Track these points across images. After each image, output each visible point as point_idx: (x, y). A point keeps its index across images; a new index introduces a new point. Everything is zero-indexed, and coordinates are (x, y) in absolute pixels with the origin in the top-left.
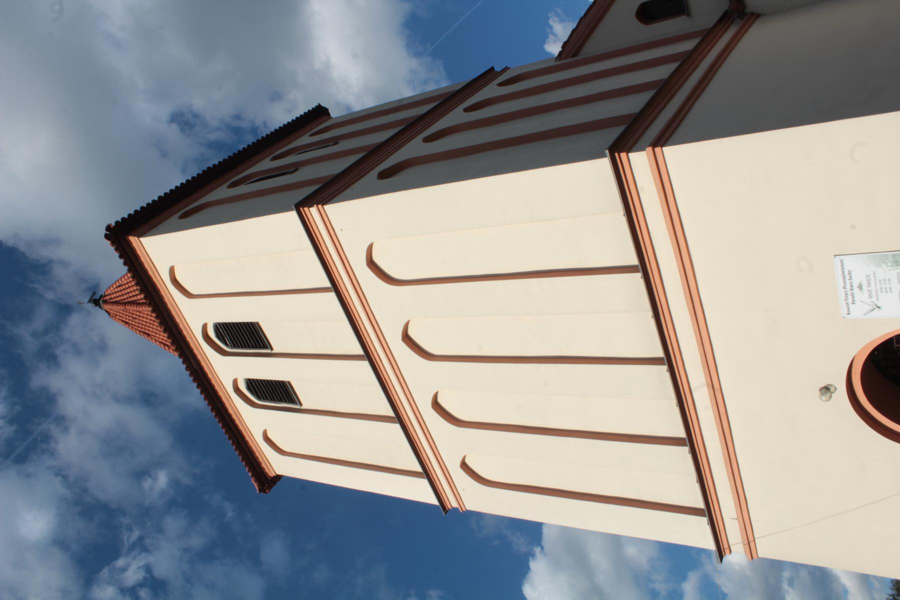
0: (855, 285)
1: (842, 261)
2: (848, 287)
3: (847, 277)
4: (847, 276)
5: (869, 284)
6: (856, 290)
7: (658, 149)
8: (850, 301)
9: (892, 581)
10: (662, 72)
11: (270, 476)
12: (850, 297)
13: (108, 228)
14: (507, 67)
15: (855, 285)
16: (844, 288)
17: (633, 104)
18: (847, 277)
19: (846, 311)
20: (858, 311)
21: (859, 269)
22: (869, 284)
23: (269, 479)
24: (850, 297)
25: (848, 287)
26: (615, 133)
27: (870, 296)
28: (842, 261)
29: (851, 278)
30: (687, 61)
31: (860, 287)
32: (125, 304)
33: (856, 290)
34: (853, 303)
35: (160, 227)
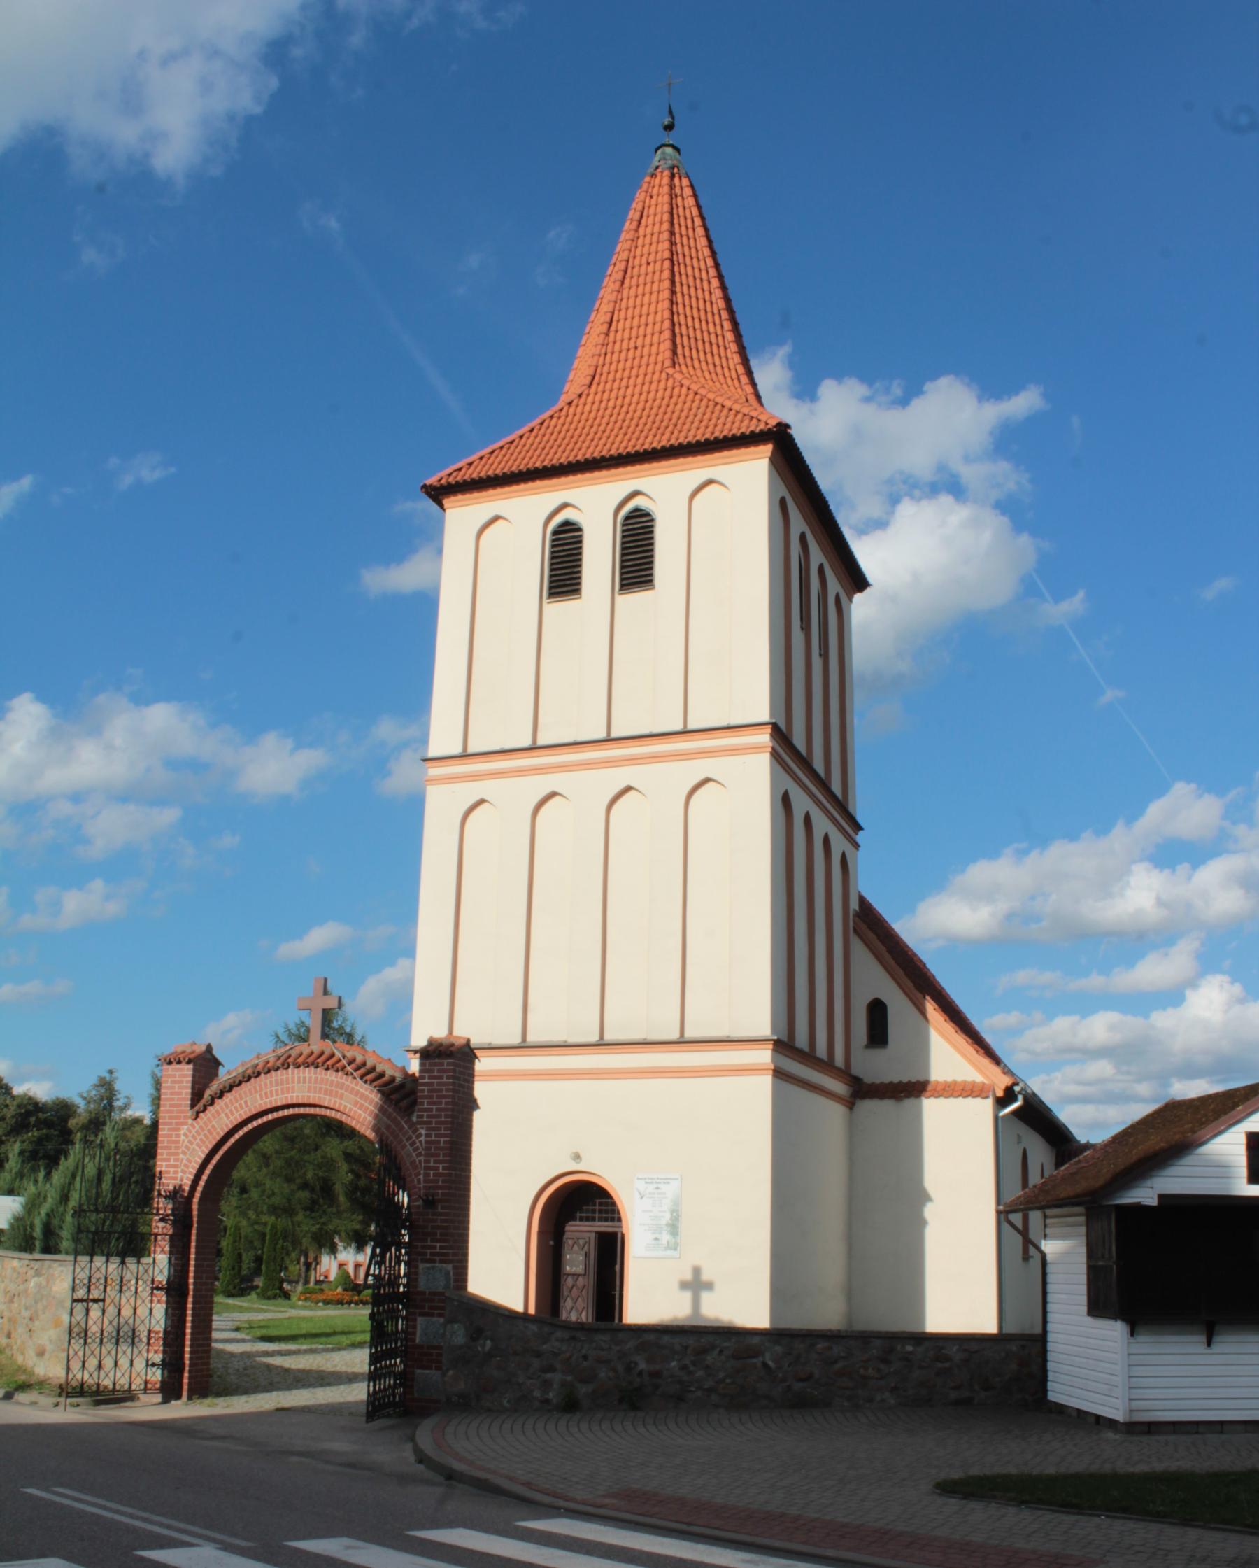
0: (659, 1185)
1: (677, 1179)
2: (658, 1181)
3: (665, 1181)
4: (667, 1181)
5: (660, 1194)
6: (656, 1185)
7: (764, 738)
8: (647, 1181)
9: (436, 590)
10: (819, 766)
11: (444, 499)
12: (650, 1181)
13: (787, 426)
14: (858, 827)
15: (659, 1185)
16: (658, 1179)
17: (799, 742)
18: (665, 1181)
19: (640, 1177)
20: (641, 1185)
21: (671, 1189)
22: (660, 1194)
23: (440, 497)
24: (650, 1181)
25: (658, 1181)
26: (783, 726)
27: (650, 1194)
28: (677, 1179)
29: (664, 1183)
30: (824, 785)
31: (657, 1188)
32: (672, 214)
33: (656, 1185)
34: (646, 1183)
35: (775, 473)
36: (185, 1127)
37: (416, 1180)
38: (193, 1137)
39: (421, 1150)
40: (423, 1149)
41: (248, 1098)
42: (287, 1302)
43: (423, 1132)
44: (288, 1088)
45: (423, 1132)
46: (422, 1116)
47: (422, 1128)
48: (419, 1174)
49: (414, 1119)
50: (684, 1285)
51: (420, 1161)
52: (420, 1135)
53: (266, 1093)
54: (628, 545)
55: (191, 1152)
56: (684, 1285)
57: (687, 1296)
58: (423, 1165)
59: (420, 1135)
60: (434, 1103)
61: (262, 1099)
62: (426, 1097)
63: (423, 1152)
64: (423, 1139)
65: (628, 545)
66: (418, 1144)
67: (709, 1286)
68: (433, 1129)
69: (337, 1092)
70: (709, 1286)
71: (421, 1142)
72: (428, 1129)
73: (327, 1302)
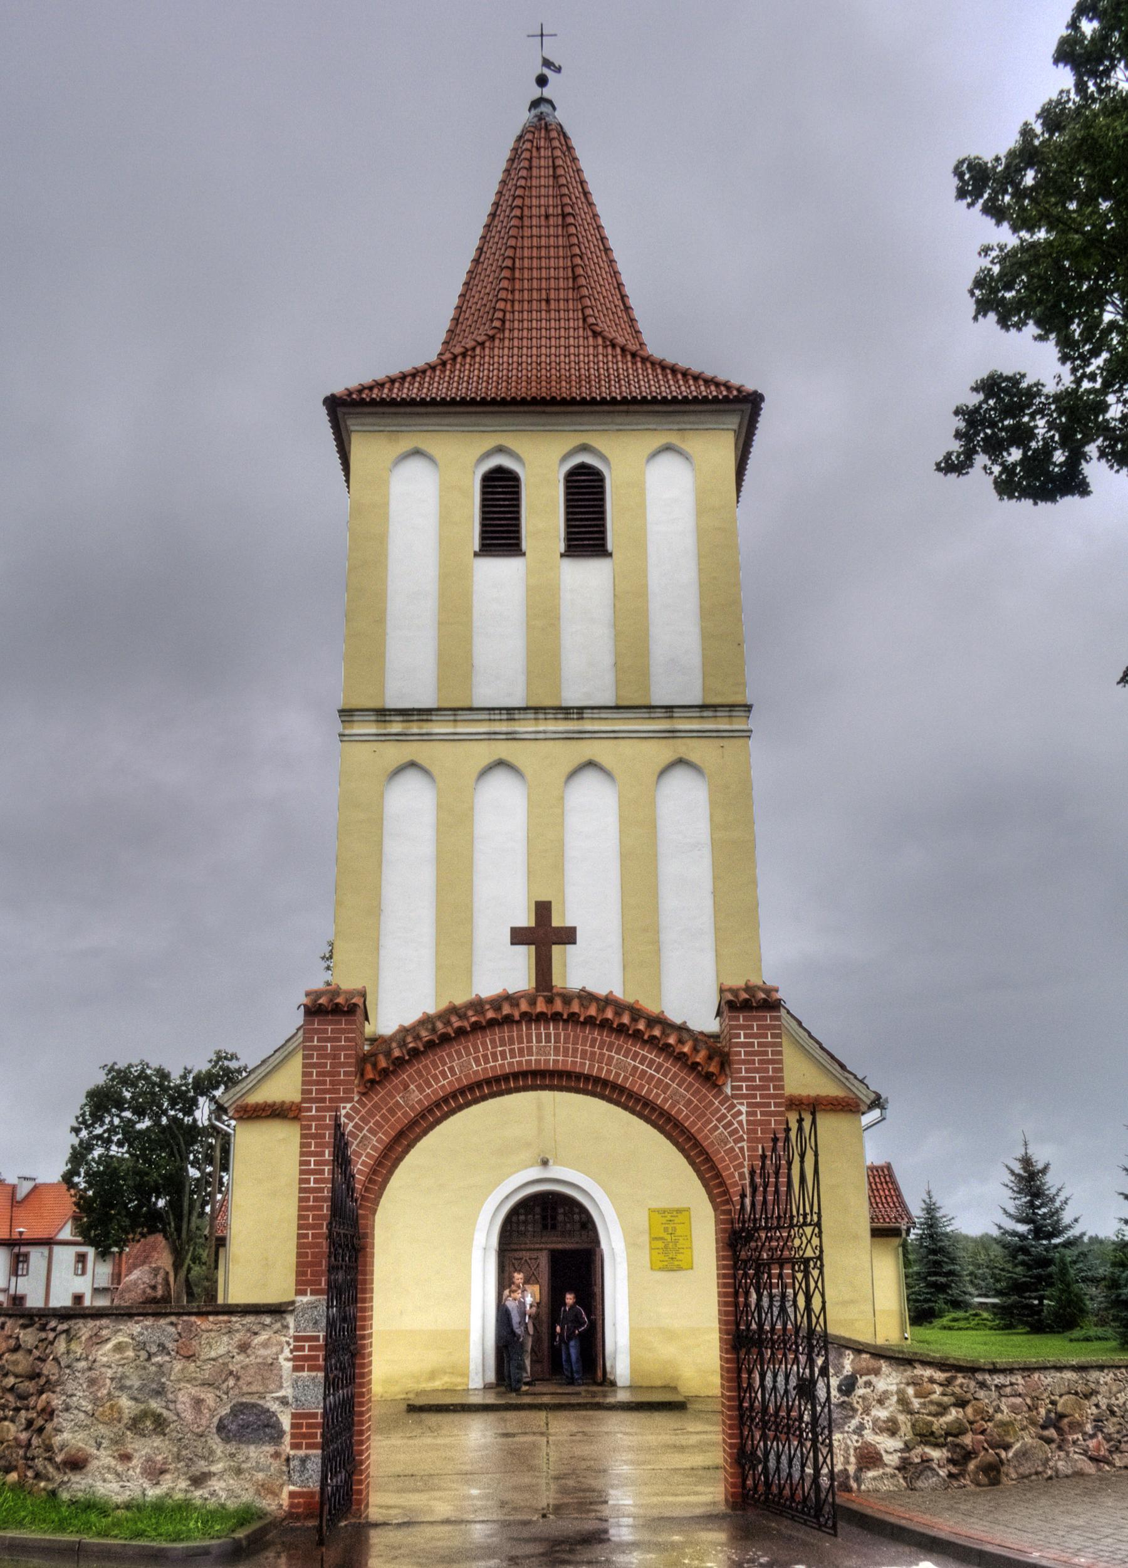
36: (349, 1106)
37: (736, 1174)
38: (362, 1119)
39: (741, 1133)
40: (744, 1132)
41: (454, 1064)
42: (411, 1402)
43: (744, 1109)
44: (521, 1050)
45: (744, 1109)
46: (740, 1088)
47: (742, 1104)
48: (741, 1165)
49: (728, 1091)
50: (519, 936)
51: (741, 1149)
52: (740, 1113)
53: (485, 1056)
54: (573, 523)
55: (360, 1142)
56: (519, 936)
57: (523, 958)
58: (746, 1154)
59: (740, 1113)
60: (757, 1071)
61: (478, 1064)
62: (744, 1062)
63: (745, 1137)
64: (743, 1118)
65: (573, 523)
66: (736, 1125)
67: (568, 936)
68: (758, 1105)
69: (602, 1055)
70: (568, 936)
71: (740, 1123)
72: (749, 1105)
73: (216, 1267)
